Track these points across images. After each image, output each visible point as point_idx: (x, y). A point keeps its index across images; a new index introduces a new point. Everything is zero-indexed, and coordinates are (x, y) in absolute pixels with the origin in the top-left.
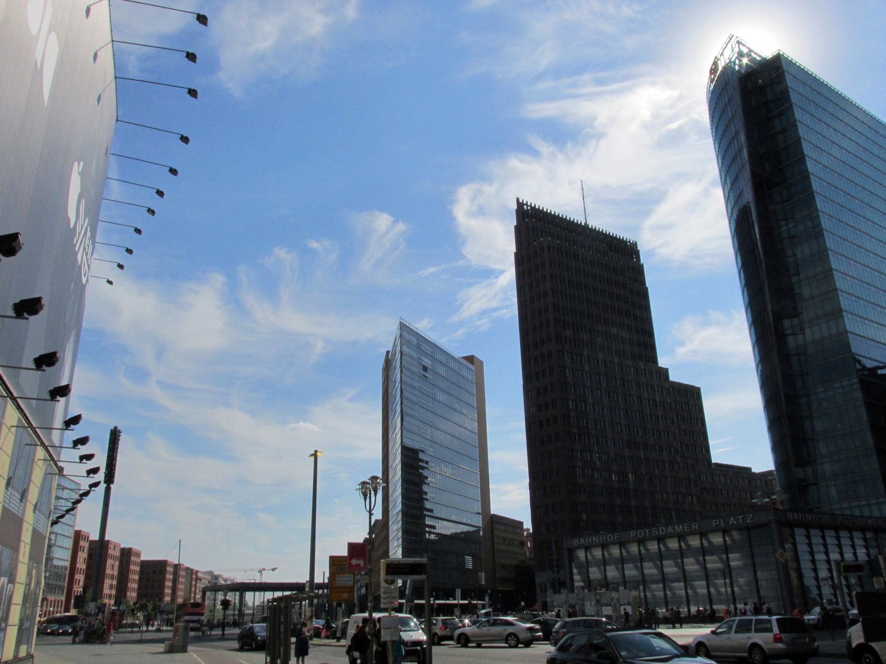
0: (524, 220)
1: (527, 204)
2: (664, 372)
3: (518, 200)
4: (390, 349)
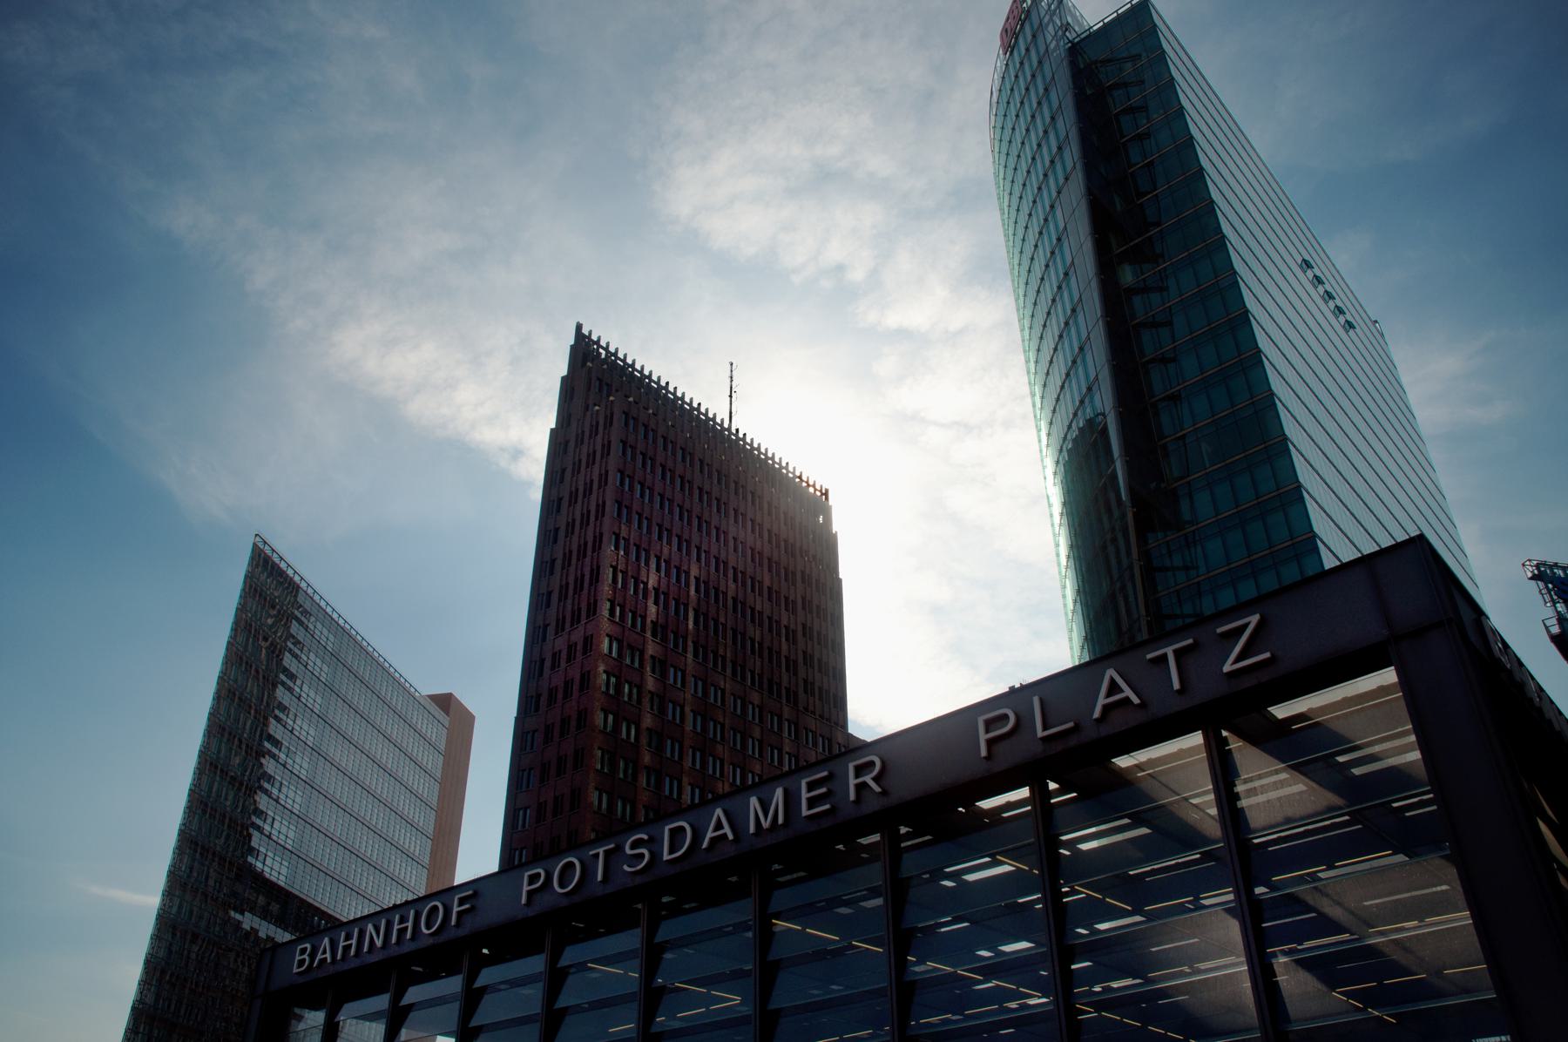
0: (584, 364)
3: (579, 327)
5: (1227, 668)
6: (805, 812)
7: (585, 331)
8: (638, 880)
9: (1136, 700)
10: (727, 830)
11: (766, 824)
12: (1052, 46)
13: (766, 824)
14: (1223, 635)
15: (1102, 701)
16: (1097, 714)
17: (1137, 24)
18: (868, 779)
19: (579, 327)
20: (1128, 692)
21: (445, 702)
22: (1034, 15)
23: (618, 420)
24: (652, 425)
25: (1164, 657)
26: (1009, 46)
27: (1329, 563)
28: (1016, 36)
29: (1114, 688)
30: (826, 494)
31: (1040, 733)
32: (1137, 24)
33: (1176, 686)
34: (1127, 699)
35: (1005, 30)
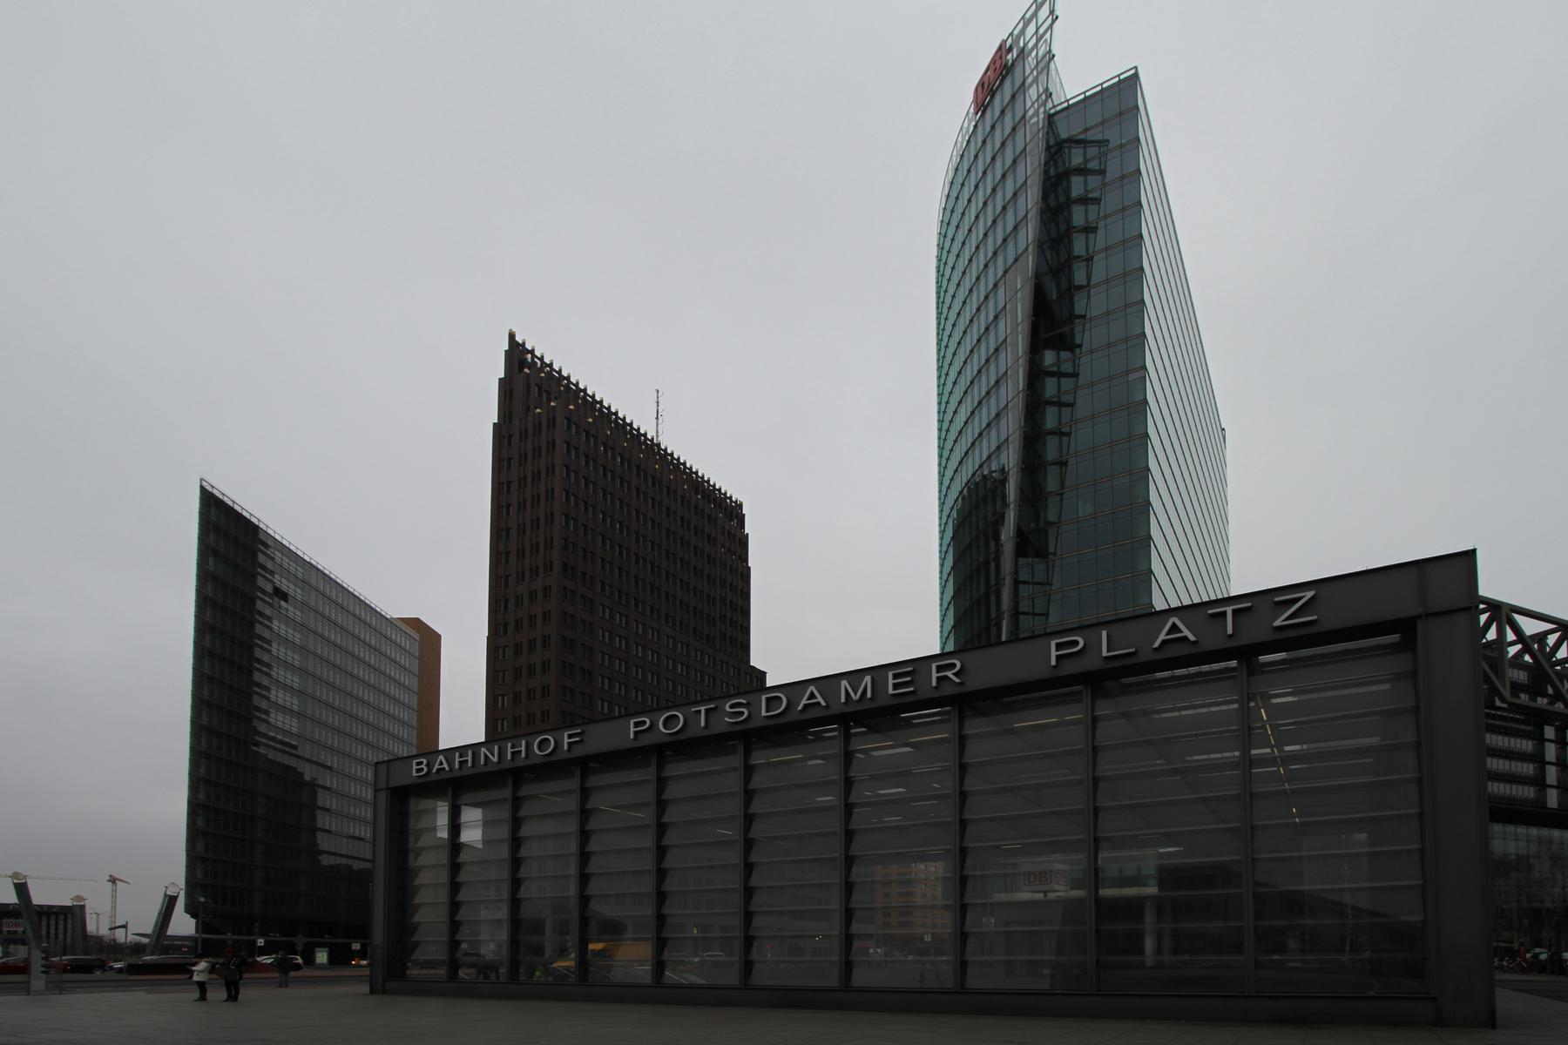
0: (521, 370)
3: (512, 336)
5: (1277, 623)
6: (891, 691)
7: (519, 339)
8: (737, 728)
9: (1192, 638)
10: (445, 765)
11: (855, 697)
12: (1030, 113)
13: (855, 697)
14: (1278, 603)
15: (804, 702)
16: (1156, 645)
17: (1121, 98)
18: (949, 674)
19: (512, 336)
20: (820, 699)
21: (416, 624)
22: (1018, 70)
23: (561, 423)
24: (593, 432)
25: (1224, 613)
26: (981, 106)
27: (1159, 604)
28: (993, 93)
29: (812, 696)
30: (741, 506)
31: (1105, 653)
32: (1121, 98)
33: (1230, 631)
34: (1185, 638)
35: (981, 84)
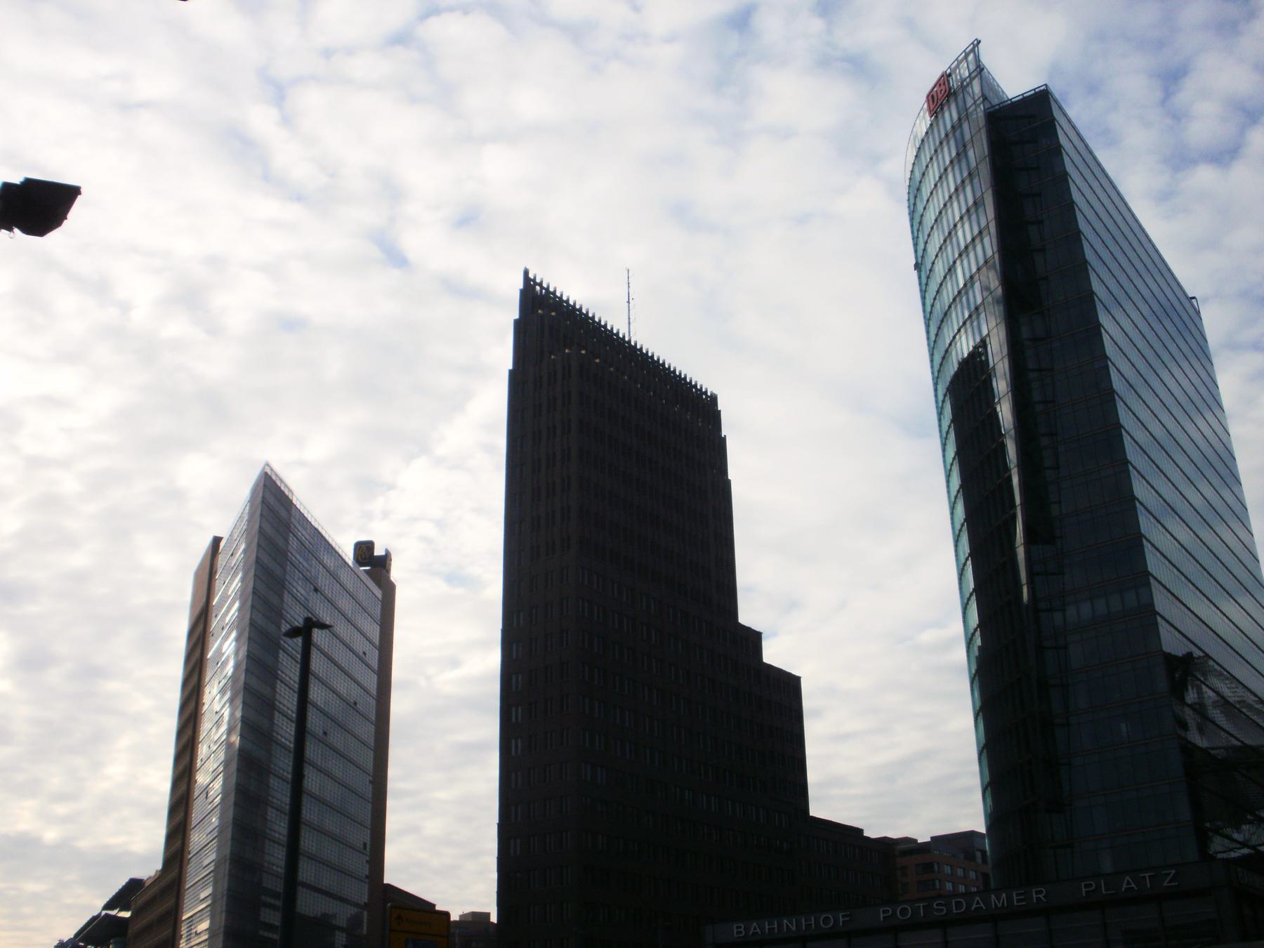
1: (540, 284)
2: (753, 639)
3: (526, 273)
4: (224, 533)
